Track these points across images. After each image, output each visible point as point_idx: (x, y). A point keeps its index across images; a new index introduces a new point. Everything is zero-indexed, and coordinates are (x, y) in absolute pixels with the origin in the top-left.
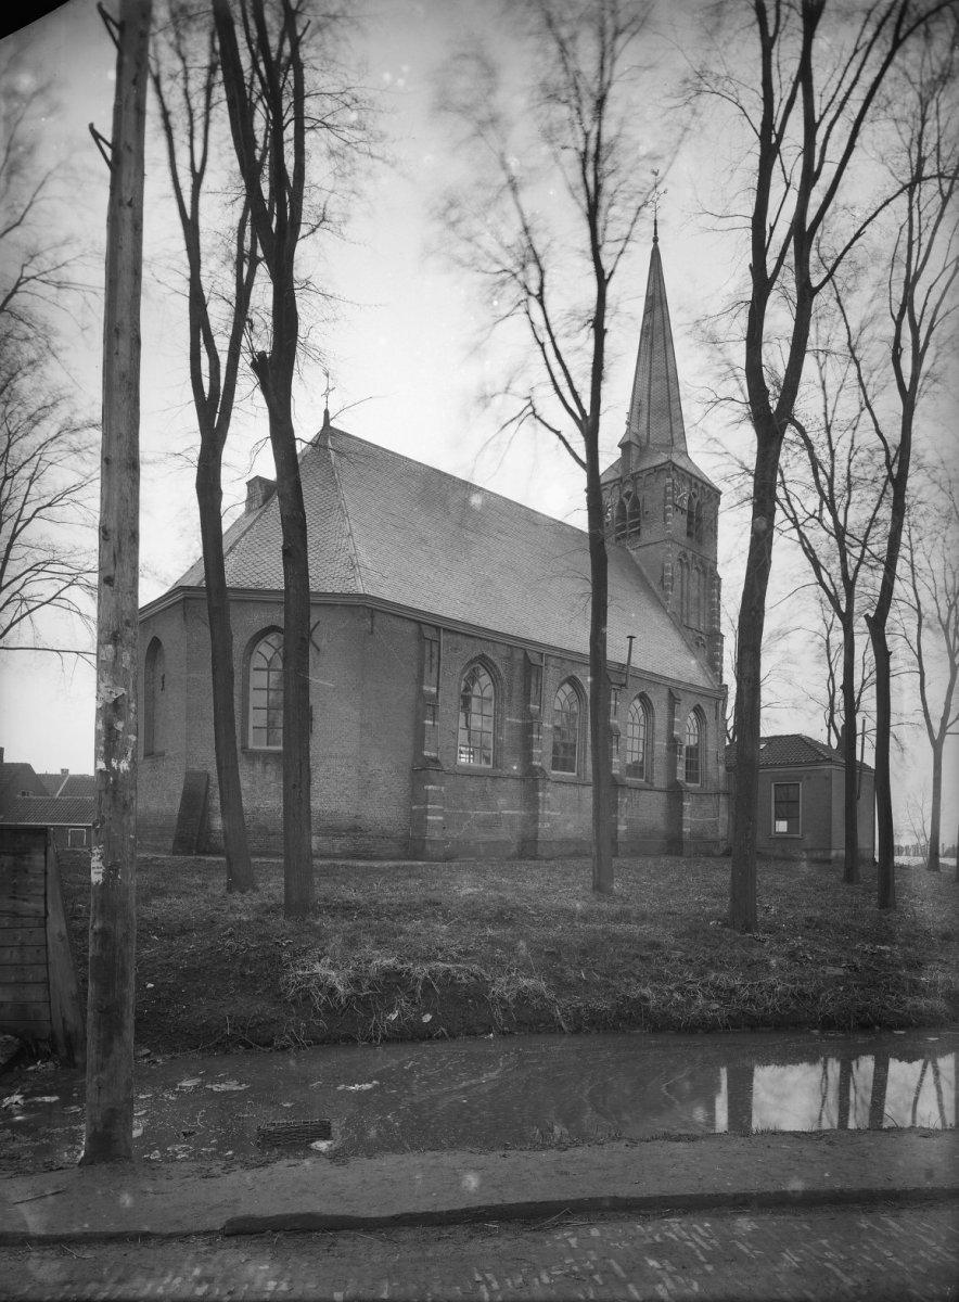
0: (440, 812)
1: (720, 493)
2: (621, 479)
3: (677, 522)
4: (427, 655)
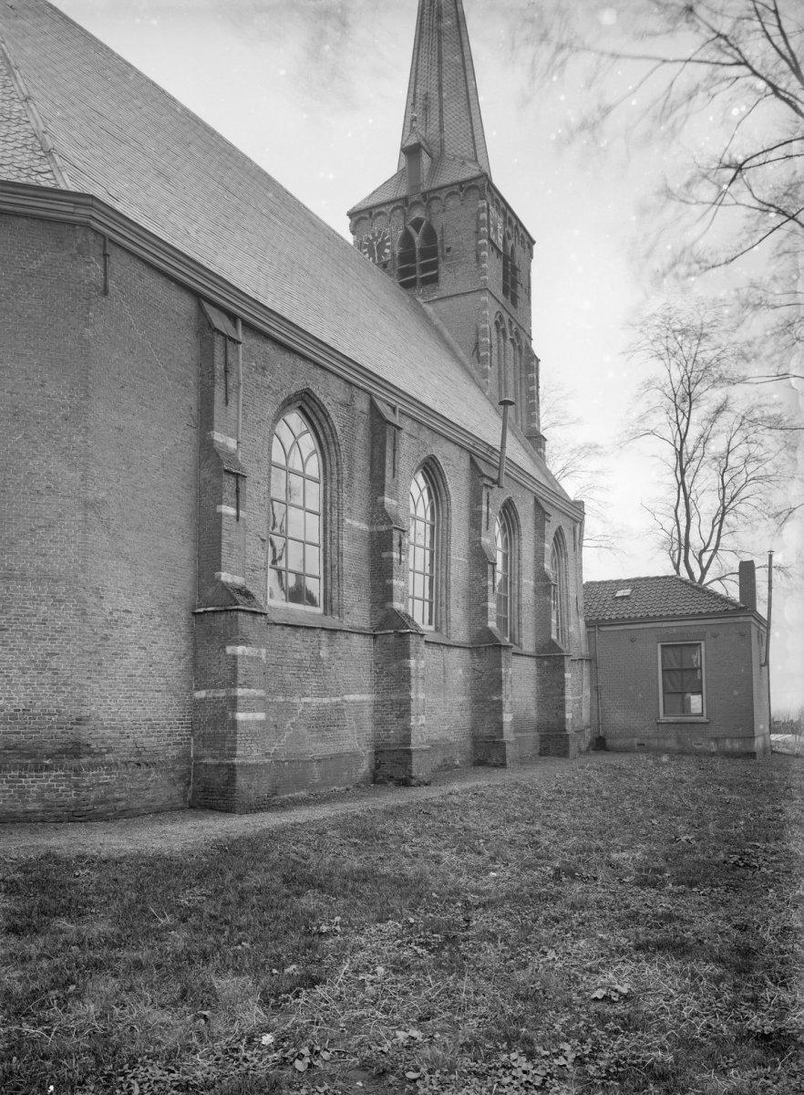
0: (264, 704)
1: (534, 242)
2: (405, 199)
3: (492, 269)
4: (219, 367)
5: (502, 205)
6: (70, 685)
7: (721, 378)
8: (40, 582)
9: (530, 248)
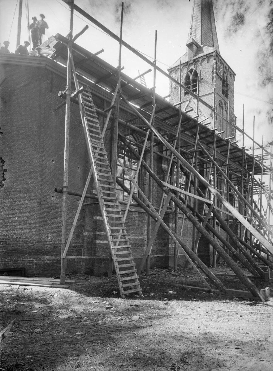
1: (235, 75)
2: (187, 63)
5: (223, 62)
6: (35, 229)
7: (225, 104)
8: (25, 193)
9: (234, 77)
